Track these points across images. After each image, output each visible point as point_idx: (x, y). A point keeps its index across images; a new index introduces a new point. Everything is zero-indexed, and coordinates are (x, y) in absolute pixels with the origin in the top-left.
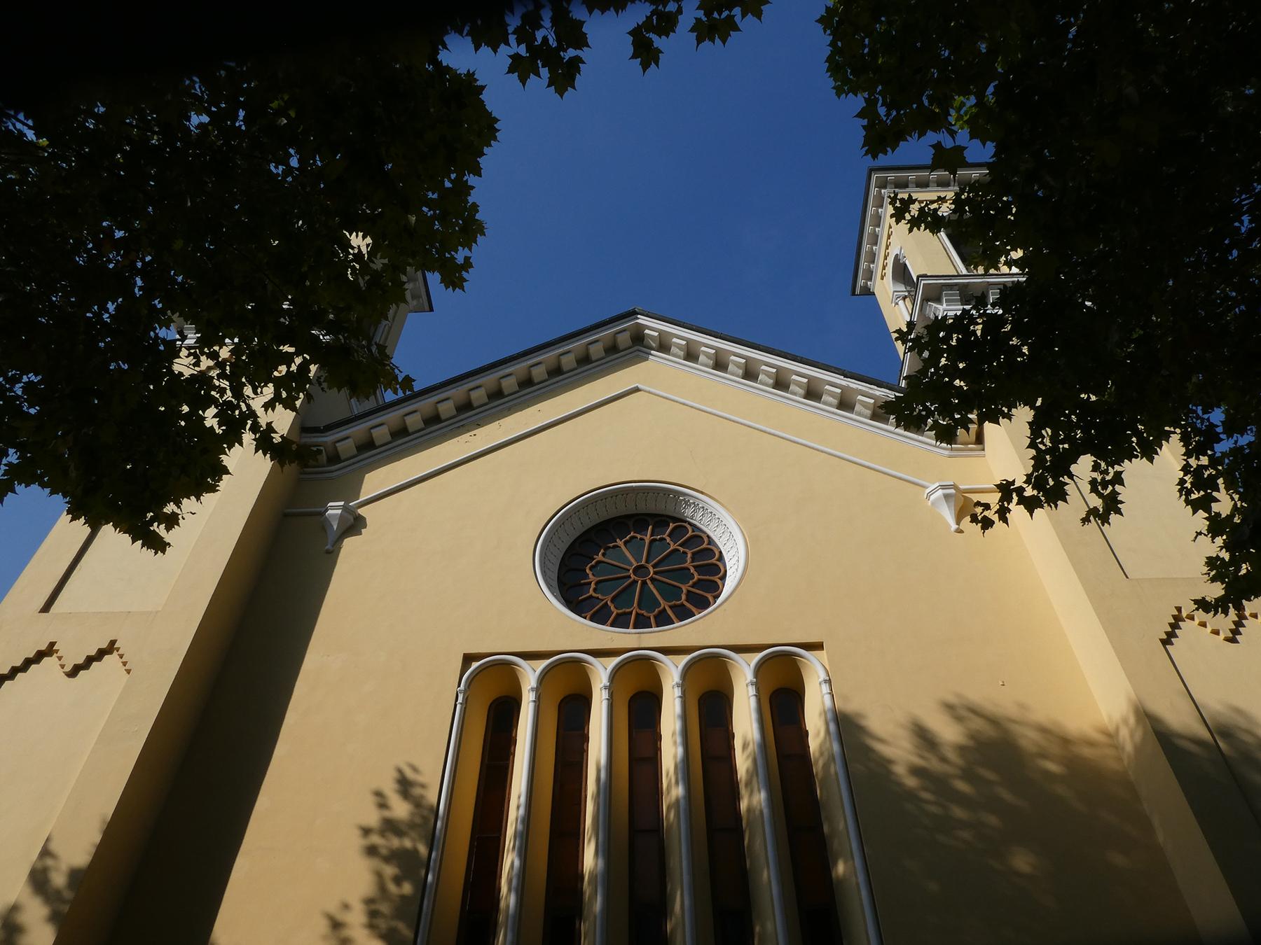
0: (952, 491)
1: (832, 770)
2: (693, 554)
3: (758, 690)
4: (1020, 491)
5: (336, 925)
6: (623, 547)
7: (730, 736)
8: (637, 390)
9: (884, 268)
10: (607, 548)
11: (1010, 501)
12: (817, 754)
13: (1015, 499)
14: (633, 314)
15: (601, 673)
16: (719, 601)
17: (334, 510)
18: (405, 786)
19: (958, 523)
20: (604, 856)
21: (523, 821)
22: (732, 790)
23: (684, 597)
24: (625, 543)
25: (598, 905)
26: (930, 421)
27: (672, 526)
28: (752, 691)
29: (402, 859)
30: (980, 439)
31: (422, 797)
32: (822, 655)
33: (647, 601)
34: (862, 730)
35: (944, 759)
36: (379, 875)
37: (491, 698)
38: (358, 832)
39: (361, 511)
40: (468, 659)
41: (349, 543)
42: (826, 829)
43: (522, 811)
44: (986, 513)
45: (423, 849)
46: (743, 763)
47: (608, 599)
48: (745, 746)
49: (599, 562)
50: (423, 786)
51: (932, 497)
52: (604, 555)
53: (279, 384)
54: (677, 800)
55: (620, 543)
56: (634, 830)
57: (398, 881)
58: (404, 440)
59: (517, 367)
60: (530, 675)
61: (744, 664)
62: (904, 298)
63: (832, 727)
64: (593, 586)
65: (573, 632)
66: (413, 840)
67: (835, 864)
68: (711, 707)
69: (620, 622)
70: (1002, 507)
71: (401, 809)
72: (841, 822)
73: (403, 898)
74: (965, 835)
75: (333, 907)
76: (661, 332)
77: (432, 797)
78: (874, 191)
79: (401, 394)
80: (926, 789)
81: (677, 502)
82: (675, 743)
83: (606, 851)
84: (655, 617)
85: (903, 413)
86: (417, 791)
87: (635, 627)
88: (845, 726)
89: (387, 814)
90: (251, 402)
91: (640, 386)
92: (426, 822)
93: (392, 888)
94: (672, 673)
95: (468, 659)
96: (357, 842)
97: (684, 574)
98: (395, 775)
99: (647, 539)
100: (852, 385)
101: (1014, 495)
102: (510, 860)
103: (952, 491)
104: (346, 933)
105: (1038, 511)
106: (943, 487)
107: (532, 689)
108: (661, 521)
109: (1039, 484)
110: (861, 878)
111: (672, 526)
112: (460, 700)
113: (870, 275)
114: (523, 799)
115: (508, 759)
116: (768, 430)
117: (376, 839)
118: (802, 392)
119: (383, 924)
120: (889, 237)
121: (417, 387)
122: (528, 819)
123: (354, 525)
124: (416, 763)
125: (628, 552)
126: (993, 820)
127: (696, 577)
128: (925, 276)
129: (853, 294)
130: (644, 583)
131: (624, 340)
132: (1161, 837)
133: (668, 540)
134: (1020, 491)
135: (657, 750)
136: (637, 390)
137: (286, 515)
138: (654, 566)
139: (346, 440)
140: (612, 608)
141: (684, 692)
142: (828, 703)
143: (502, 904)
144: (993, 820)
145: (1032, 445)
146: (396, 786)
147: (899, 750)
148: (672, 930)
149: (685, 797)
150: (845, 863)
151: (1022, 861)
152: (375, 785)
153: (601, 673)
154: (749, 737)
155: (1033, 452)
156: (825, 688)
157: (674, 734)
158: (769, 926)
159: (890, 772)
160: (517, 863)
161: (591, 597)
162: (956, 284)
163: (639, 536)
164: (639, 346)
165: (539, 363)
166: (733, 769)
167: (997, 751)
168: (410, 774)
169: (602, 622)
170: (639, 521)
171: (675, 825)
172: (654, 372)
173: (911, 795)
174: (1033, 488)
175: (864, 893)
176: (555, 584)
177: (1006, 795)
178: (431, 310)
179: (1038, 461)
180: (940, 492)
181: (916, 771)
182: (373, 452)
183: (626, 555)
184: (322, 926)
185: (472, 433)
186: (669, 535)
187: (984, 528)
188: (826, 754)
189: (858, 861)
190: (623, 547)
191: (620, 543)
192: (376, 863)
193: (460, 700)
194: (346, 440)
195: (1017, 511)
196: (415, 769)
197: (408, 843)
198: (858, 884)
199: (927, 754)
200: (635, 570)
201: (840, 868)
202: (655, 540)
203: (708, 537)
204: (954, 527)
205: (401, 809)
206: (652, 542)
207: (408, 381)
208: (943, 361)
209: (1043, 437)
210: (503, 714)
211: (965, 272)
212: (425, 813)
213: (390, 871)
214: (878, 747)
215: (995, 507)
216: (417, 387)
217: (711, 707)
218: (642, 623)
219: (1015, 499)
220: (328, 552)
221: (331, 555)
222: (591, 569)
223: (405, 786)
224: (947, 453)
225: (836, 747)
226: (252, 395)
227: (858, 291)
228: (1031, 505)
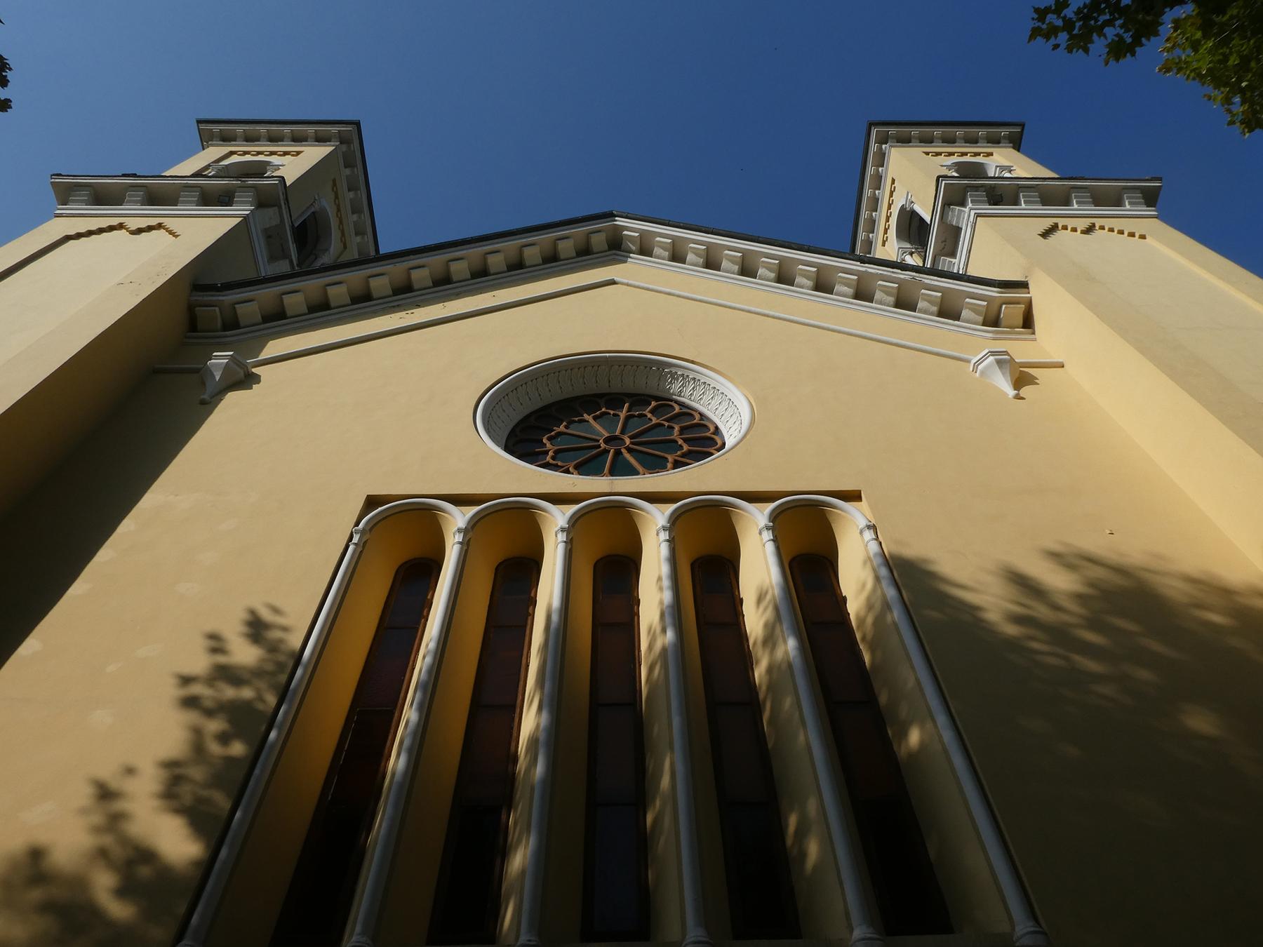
1: (889, 618)
5: (105, 793)
6: (591, 421)
9: (887, 220)
10: (570, 423)
14: (610, 215)
15: (556, 520)
18: (257, 628)
20: (551, 712)
22: (745, 659)
27: (653, 404)
32: (864, 504)
34: (933, 576)
35: (1056, 608)
36: (197, 732)
37: (399, 540)
41: (233, 399)
42: (883, 699)
46: (754, 621)
50: (285, 629)
52: (566, 427)
54: (664, 650)
56: (596, 705)
57: (224, 739)
58: (321, 312)
60: (457, 520)
63: (884, 572)
64: (551, 453)
67: (903, 734)
71: (245, 654)
73: (230, 761)
75: (107, 771)
76: (643, 234)
78: (873, 147)
83: (557, 704)
88: (905, 575)
89: (221, 659)
92: (286, 672)
93: (215, 748)
94: (654, 527)
96: (172, 692)
106: (993, 353)
107: (459, 530)
108: (640, 400)
110: (948, 736)
111: (653, 404)
117: (197, 689)
120: (891, 195)
123: (246, 380)
124: (278, 603)
126: (1144, 674)
127: (686, 448)
130: (618, 453)
131: (599, 241)
138: (631, 438)
139: (251, 304)
142: (873, 547)
144: (1144, 674)
146: (244, 629)
148: (656, 821)
149: (675, 645)
150: (922, 728)
151: (1201, 722)
152: (210, 627)
153: (556, 520)
156: (869, 535)
157: (660, 579)
158: (812, 806)
162: (982, 186)
164: (616, 249)
168: (266, 615)
172: (632, 269)
173: (1011, 644)
175: (958, 761)
177: (1156, 646)
180: (991, 358)
181: (1018, 620)
182: (278, 320)
184: (83, 794)
189: (942, 719)
190: (591, 421)
192: (192, 717)
193: (356, 539)
196: (276, 611)
198: (945, 751)
200: (607, 441)
202: (634, 416)
204: (1011, 392)
205: (245, 654)
206: (628, 418)
210: (419, 573)
212: (282, 658)
220: (203, 403)
221: (207, 405)
225: (891, 593)
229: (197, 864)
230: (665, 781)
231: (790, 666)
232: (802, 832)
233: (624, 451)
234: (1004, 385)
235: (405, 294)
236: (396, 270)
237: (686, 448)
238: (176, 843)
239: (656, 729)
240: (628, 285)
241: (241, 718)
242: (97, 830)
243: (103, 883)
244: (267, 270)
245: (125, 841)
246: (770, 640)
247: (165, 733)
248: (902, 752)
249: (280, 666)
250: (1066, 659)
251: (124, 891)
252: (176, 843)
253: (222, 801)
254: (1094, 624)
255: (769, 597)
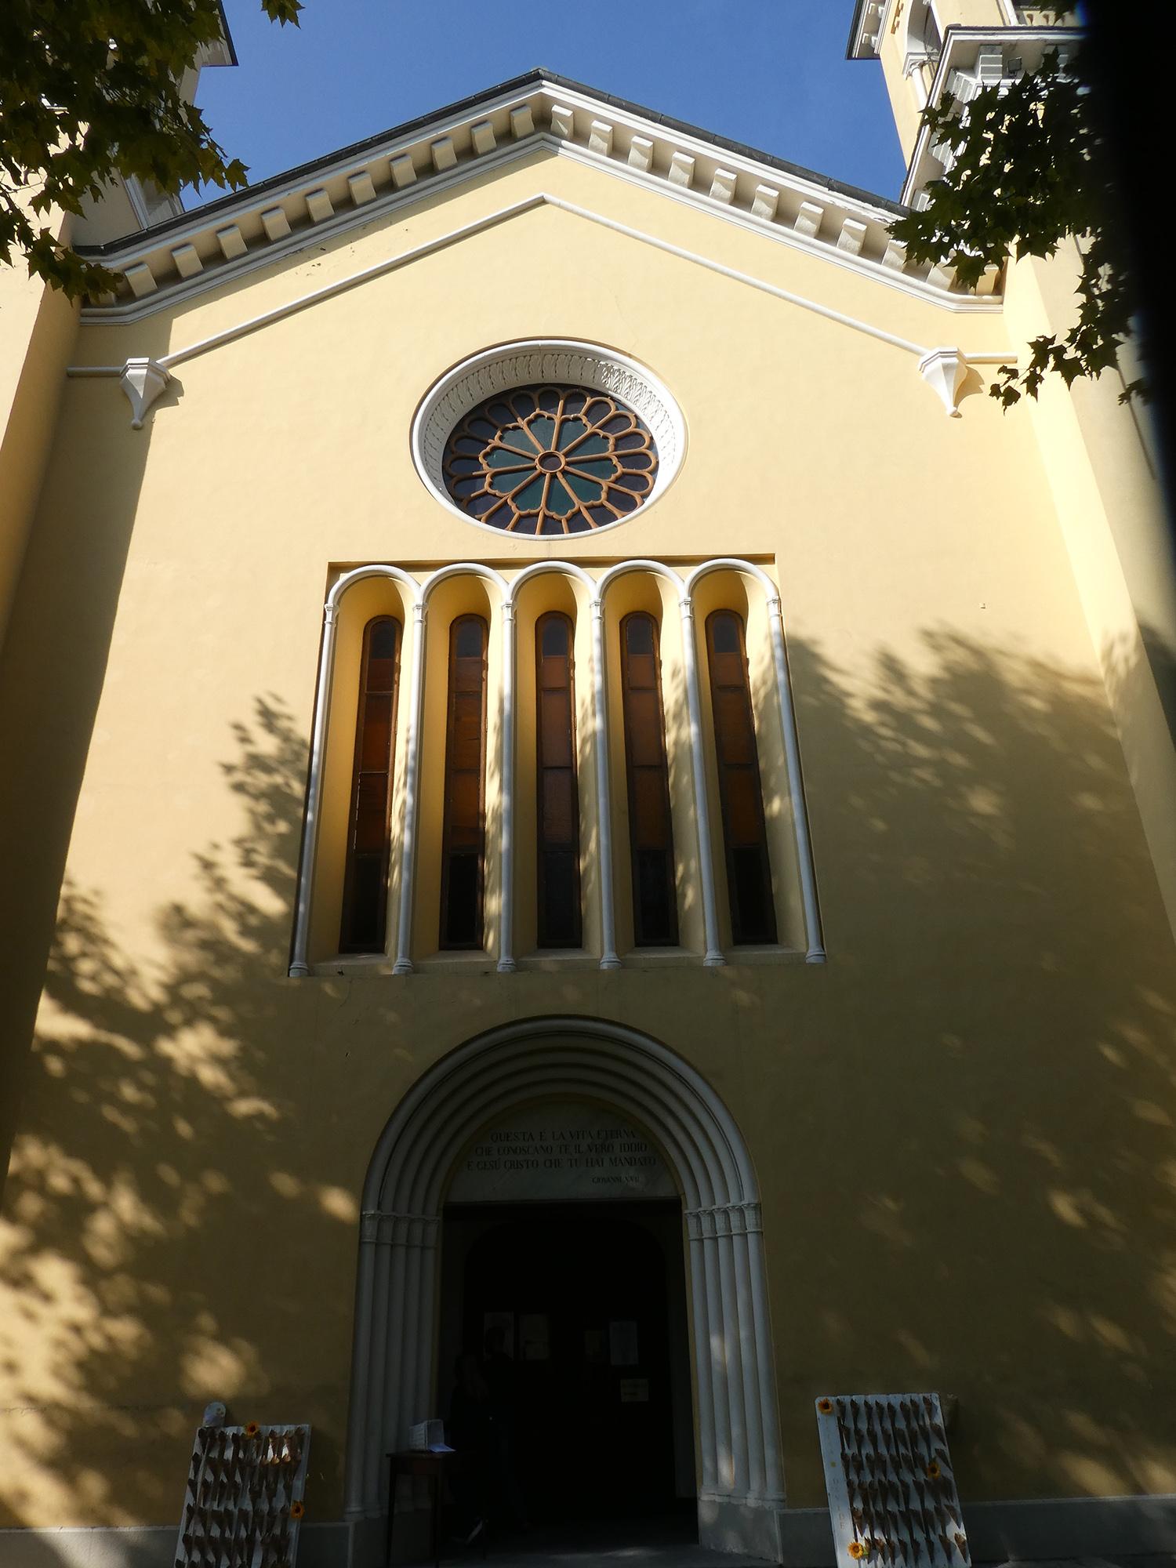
0: (955, 360)
2: (617, 439)
3: (692, 611)
4: (1061, 350)
5: (208, 865)
6: (526, 429)
7: (655, 665)
8: (542, 202)
9: (898, 14)
11: (1044, 366)
12: (758, 684)
13: (1052, 362)
14: (535, 78)
16: (648, 501)
17: (137, 369)
18: (269, 718)
19: (956, 404)
20: (509, 794)
21: (414, 757)
22: (658, 725)
23: (604, 495)
24: (529, 423)
25: (504, 842)
26: (952, 252)
27: (589, 401)
28: (686, 611)
29: (277, 799)
30: (999, 288)
31: (290, 730)
33: (557, 499)
34: (816, 658)
35: (911, 693)
38: (220, 770)
39: (174, 372)
40: (335, 569)
41: (163, 417)
42: (762, 765)
43: (412, 746)
44: (1012, 383)
45: (298, 788)
47: (508, 497)
48: (675, 674)
49: (495, 448)
50: (290, 718)
51: (928, 369)
52: (501, 438)
53: (56, 167)
54: (594, 734)
55: (522, 423)
56: (542, 767)
58: (219, 269)
59: (374, 159)
60: (413, 590)
61: (677, 579)
62: (922, 66)
63: (779, 653)
64: (488, 479)
65: (468, 538)
66: (286, 777)
67: (770, 801)
68: (636, 630)
69: (524, 525)
70: (1033, 373)
71: (267, 744)
72: (779, 758)
74: (925, 774)
76: (577, 112)
77: (303, 730)
79: (229, 191)
80: (883, 724)
81: (596, 369)
82: (592, 670)
83: (513, 787)
84: (568, 520)
85: (920, 241)
86: (283, 724)
87: (542, 533)
88: (796, 655)
89: (250, 749)
90: (12, 196)
91: (547, 197)
94: (588, 588)
95: (335, 569)
97: (602, 465)
98: (256, 706)
99: (558, 418)
100: (839, 203)
101: (1051, 359)
102: (401, 797)
103: (955, 360)
104: (220, 872)
105: (1078, 378)
106: (945, 354)
108: (575, 393)
109: (1084, 345)
110: (797, 815)
111: (589, 401)
112: (329, 618)
113: (875, 27)
114: (413, 732)
115: (391, 688)
116: (721, 267)
118: (770, 211)
119: (262, 859)
121: (253, 178)
122: (420, 754)
123: (167, 392)
124: (280, 693)
125: (530, 432)
126: (958, 759)
127: (620, 469)
128: (957, 27)
129: (849, 57)
130: (554, 477)
131: (523, 121)
132: (1134, 778)
133: (585, 420)
134: (1061, 350)
135: (569, 679)
136: (542, 202)
137: (71, 376)
138: (566, 455)
140: (513, 508)
141: (603, 612)
143: (395, 844)
144: (958, 759)
145: (1084, 288)
147: (858, 682)
148: (586, 869)
150: (782, 799)
151: (982, 802)
153: (501, 589)
154: (680, 664)
155: (1082, 298)
156: (774, 609)
157: (591, 660)
158: (693, 864)
159: (844, 706)
160: (410, 800)
161: (486, 493)
162: (1001, 43)
163: (546, 414)
164: (544, 130)
165: (444, 139)
166: (658, 701)
167: (974, 682)
168: (273, 706)
169: (502, 525)
170: (547, 393)
171: (591, 760)
172: (562, 173)
173: (866, 730)
174: (1077, 348)
176: (440, 476)
178: (235, 63)
179: (1088, 309)
180: (940, 361)
181: (878, 706)
183: (530, 438)
184: (194, 867)
185: (315, 261)
186: (586, 414)
187: (1007, 403)
188: (770, 683)
189: (795, 798)
191: (522, 423)
193: (329, 618)
194: (138, 266)
195: (1052, 378)
196: (278, 700)
197: (278, 779)
199: (893, 688)
200: (544, 459)
201: (775, 806)
202: (567, 420)
203: (636, 417)
206: (564, 422)
207: (238, 170)
208: (984, 160)
209: (1099, 277)
210: (382, 636)
211: (1014, 22)
212: (296, 747)
213: (263, 807)
214: (834, 677)
215: (1024, 374)
216: (253, 178)
217: (636, 630)
218: (550, 527)
219: (1052, 362)
220: (136, 428)
221: (142, 431)
222: (485, 456)
223: (269, 718)
224: (953, 306)
225: (781, 676)
226: (13, 186)
227: (856, 53)
228: (1069, 370)
229: (286, 916)
230: (593, 845)
231: (690, 746)
232: (685, 879)
233: (559, 475)
234: (944, 391)
235: (307, 233)
236: (289, 198)
237: (620, 469)
238: (270, 903)
239: (587, 799)
240: (559, 206)
241: (277, 799)
242: (210, 891)
243: (229, 929)
244: (149, 221)
245: (233, 898)
246: (677, 716)
247: (231, 817)
248: (767, 812)
249: (298, 756)
250: (904, 744)
251: (246, 931)
252: (270, 903)
253: (290, 872)
254: (936, 710)
255: (681, 676)
